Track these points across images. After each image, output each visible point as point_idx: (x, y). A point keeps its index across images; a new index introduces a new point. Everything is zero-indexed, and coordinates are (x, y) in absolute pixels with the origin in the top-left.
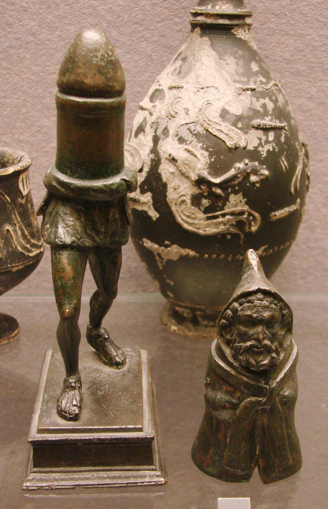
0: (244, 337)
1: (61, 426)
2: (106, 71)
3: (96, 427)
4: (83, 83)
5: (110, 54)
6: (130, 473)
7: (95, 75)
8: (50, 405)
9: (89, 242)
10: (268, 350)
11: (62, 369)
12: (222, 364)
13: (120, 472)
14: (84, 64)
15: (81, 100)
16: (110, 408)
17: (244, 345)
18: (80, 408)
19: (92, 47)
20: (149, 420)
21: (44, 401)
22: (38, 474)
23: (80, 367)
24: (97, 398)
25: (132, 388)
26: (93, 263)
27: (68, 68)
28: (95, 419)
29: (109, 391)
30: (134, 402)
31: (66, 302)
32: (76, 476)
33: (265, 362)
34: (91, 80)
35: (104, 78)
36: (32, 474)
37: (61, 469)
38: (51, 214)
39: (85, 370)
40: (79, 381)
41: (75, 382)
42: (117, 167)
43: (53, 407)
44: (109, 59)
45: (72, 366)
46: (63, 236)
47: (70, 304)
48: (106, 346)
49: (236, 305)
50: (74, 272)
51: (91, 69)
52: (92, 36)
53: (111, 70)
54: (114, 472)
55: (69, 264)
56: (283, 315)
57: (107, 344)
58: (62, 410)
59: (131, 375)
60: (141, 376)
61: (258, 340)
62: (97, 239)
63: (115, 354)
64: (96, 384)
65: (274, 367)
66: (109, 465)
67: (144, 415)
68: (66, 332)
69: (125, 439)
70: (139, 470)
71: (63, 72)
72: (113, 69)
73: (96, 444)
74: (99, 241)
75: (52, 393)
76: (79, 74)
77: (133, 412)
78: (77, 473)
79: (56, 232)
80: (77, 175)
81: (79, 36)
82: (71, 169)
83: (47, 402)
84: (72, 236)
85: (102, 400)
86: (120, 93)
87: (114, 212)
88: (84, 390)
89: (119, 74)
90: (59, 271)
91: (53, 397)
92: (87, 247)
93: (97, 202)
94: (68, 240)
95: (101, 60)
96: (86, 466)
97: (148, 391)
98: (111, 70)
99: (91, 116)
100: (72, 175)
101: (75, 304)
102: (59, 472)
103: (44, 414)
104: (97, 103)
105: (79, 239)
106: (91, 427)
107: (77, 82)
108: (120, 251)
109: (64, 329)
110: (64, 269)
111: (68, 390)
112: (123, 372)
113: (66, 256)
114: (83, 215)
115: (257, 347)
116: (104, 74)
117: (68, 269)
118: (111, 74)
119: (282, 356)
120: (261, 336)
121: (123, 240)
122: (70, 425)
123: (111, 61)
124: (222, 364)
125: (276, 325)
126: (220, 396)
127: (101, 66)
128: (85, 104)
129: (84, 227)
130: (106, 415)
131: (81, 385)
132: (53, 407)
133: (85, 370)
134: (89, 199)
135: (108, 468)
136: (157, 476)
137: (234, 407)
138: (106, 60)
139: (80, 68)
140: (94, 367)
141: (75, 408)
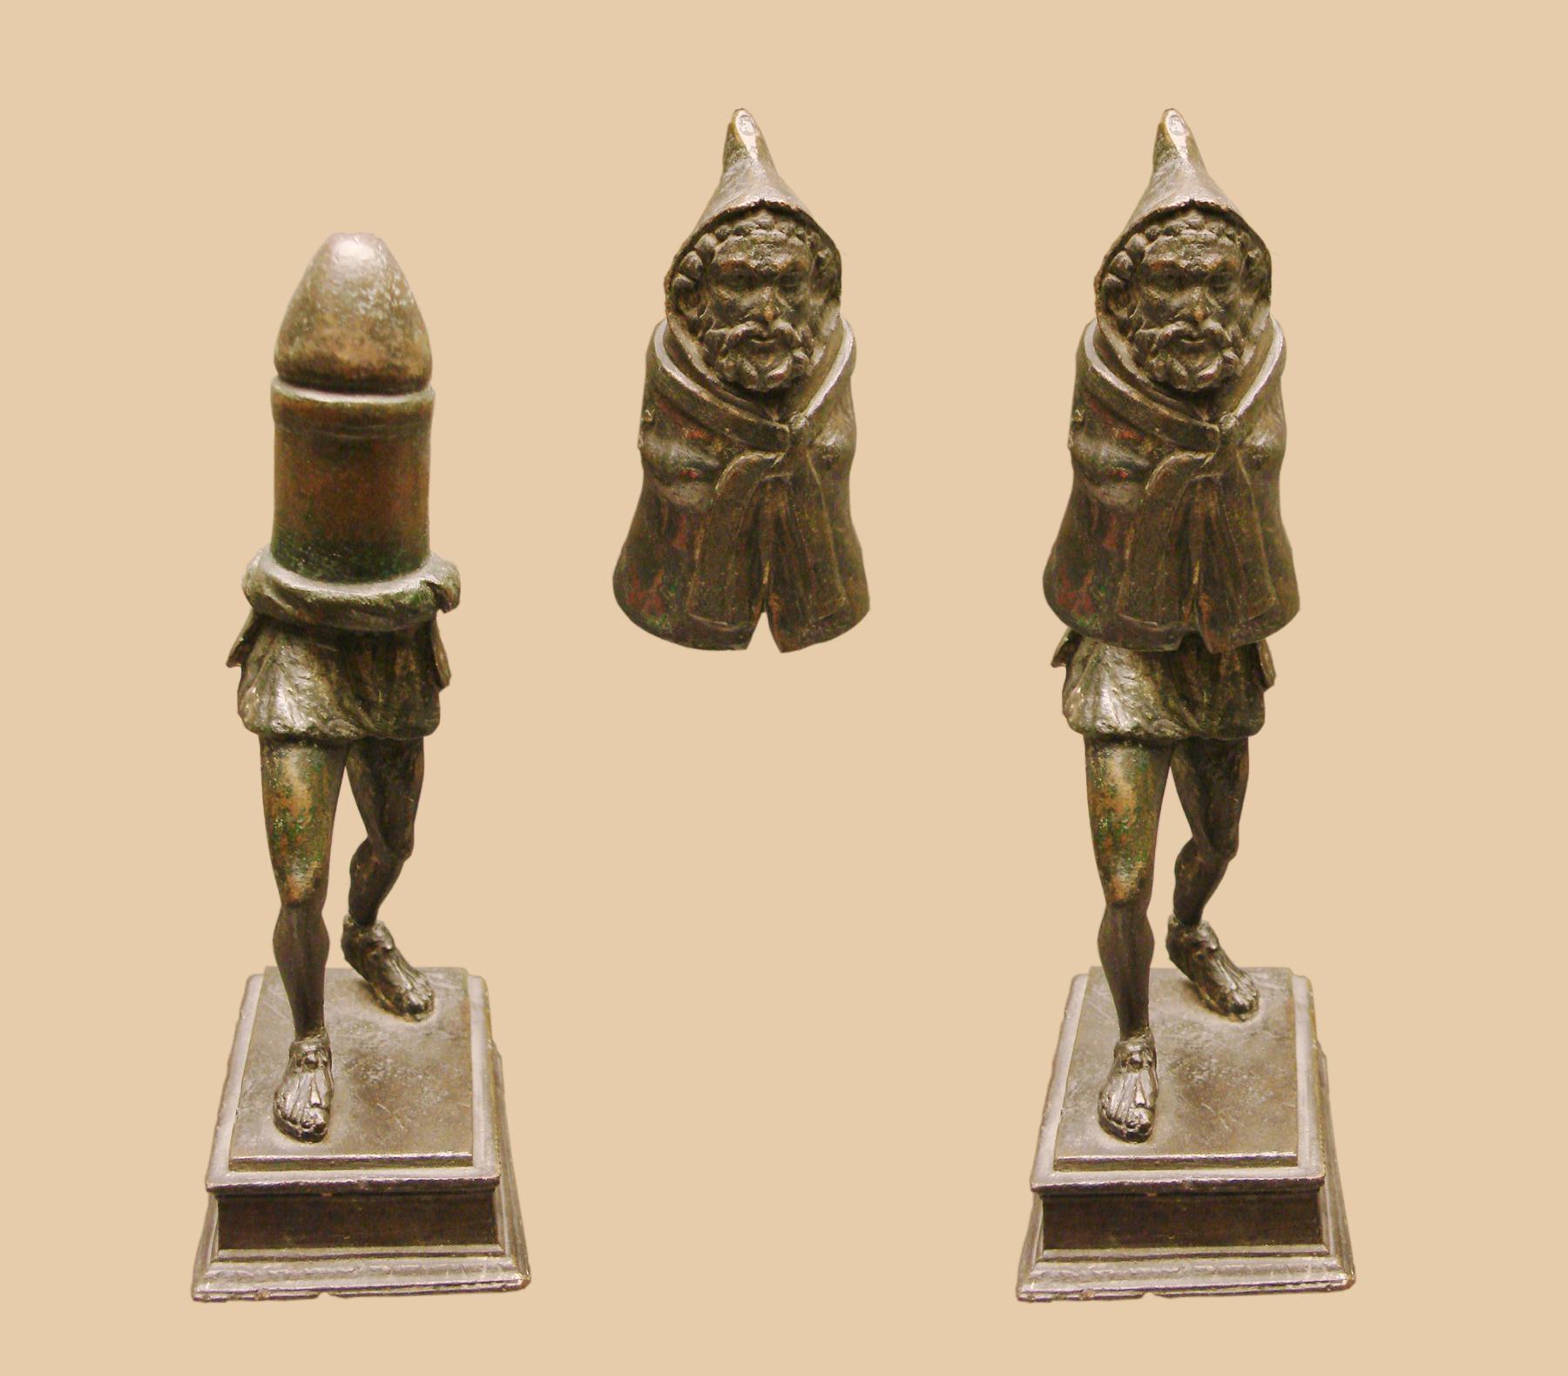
0: (730, 314)
1: (1110, 1152)
2: (387, 332)
3: (364, 1156)
4: (334, 359)
5: (397, 292)
6: (443, 1262)
7: (362, 341)
8: (258, 1104)
9: (348, 728)
10: (786, 343)
11: (286, 1021)
12: (680, 377)
13: (1245, 1260)
14: (336, 316)
15: (329, 399)
16: (396, 1111)
17: (729, 332)
18: (1152, 1110)
19: (355, 276)
20: (487, 1139)
21: (1068, 1094)
22: (1056, 1265)
23: (1153, 1015)
24: (367, 1088)
25: (1272, 1066)
26: (1183, 776)
27: (300, 325)
28: (362, 1138)
29: (1219, 1071)
30: (452, 1098)
31: (1120, 867)
32: (319, 1268)
33: (1210, 370)
34: (352, 354)
35: (382, 348)
36: (216, 1265)
37: (1109, 1252)
38: (1084, 662)
39: (1163, 1023)
40: (1150, 1048)
41: (315, 1053)
42: (414, 557)
43: (265, 1109)
44: (395, 304)
45: (1133, 1014)
46: (288, 714)
47: (305, 870)
48: (1211, 969)
49: (709, 239)
50: (315, 796)
51: (353, 328)
52: (354, 253)
53: (398, 331)
54: (406, 1260)
55: (1128, 779)
56: (1249, 262)
57: (389, 963)
58: (1110, 1117)
59: (445, 1035)
60: (469, 1039)
61: (762, 320)
62: (1192, 721)
63: (409, 986)
64: (1189, 1056)
65: (1230, 382)
66: (395, 1244)
67: (476, 1129)
68: (1120, 936)
69: (431, 1184)
70: (1288, 1255)
71: (290, 334)
72: (403, 327)
73: (1188, 1194)
74: (372, 726)
75: (262, 1077)
76: (324, 339)
77: (1274, 1120)
78: (321, 1262)
79: (1097, 704)
80: (320, 573)
81: (325, 252)
82: (306, 558)
83: (1076, 1098)
84: (308, 715)
85: (377, 1093)
86: (420, 383)
87: (406, 659)
88: (337, 1069)
89: (417, 339)
90: (1103, 795)
91: (265, 1087)
92: (1167, 738)
93: (368, 635)
94: (1125, 724)
95: (377, 306)
96: (341, 1246)
97: (484, 1072)
98: (398, 331)
99: (352, 437)
100: (310, 572)
101: (316, 871)
102: (280, 1260)
103: (1070, 1126)
104: (366, 409)
105: (325, 721)
106: (1176, 1156)
107: (320, 358)
108: (1244, 749)
109: (1116, 930)
110: (1114, 790)
111: (299, 1070)
112: (1251, 1027)
113: (295, 759)
114: (333, 666)
115: (760, 337)
116: (382, 340)
117: (1126, 792)
118: (400, 338)
119: (1248, 355)
120: (1199, 312)
121: (1251, 722)
122: (1131, 1150)
123: (399, 309)
124: (680, 377)
125: (1234, 286)
126: (1108, 452)
127: (377, 320)
128: (339, 409)
129: (1163, 692)
130: (387, 1127)
131: (330, 1057)
132: (265, 1109)
133: (1163, 1023)
134: (349, 627)
135: (1216, 1250)
136: (1331, 1269)
137: (710, 475)
138: (387, 306)
139: (326, 324)
140: (1185, 1017)
141: (1141, 1111)
